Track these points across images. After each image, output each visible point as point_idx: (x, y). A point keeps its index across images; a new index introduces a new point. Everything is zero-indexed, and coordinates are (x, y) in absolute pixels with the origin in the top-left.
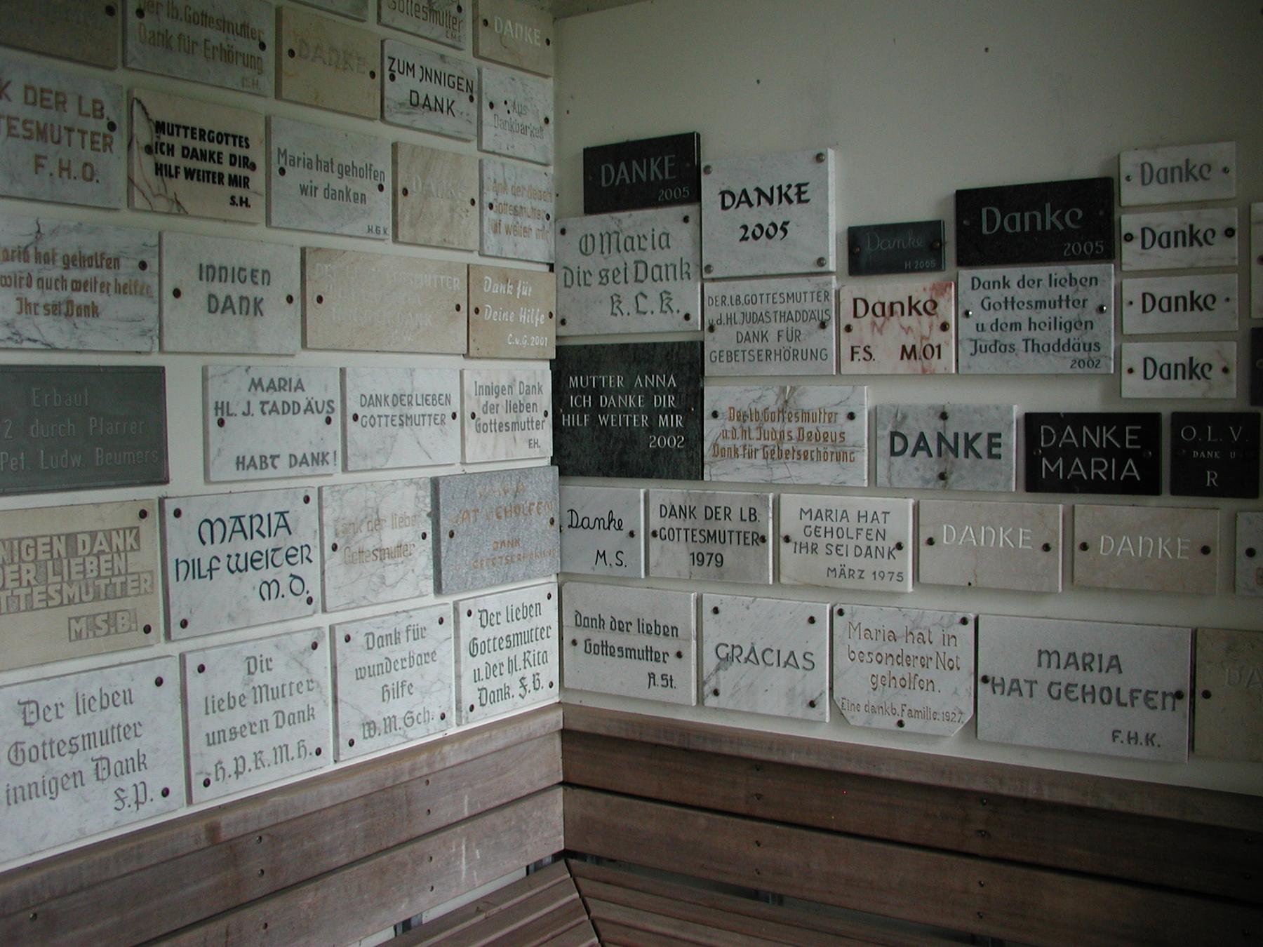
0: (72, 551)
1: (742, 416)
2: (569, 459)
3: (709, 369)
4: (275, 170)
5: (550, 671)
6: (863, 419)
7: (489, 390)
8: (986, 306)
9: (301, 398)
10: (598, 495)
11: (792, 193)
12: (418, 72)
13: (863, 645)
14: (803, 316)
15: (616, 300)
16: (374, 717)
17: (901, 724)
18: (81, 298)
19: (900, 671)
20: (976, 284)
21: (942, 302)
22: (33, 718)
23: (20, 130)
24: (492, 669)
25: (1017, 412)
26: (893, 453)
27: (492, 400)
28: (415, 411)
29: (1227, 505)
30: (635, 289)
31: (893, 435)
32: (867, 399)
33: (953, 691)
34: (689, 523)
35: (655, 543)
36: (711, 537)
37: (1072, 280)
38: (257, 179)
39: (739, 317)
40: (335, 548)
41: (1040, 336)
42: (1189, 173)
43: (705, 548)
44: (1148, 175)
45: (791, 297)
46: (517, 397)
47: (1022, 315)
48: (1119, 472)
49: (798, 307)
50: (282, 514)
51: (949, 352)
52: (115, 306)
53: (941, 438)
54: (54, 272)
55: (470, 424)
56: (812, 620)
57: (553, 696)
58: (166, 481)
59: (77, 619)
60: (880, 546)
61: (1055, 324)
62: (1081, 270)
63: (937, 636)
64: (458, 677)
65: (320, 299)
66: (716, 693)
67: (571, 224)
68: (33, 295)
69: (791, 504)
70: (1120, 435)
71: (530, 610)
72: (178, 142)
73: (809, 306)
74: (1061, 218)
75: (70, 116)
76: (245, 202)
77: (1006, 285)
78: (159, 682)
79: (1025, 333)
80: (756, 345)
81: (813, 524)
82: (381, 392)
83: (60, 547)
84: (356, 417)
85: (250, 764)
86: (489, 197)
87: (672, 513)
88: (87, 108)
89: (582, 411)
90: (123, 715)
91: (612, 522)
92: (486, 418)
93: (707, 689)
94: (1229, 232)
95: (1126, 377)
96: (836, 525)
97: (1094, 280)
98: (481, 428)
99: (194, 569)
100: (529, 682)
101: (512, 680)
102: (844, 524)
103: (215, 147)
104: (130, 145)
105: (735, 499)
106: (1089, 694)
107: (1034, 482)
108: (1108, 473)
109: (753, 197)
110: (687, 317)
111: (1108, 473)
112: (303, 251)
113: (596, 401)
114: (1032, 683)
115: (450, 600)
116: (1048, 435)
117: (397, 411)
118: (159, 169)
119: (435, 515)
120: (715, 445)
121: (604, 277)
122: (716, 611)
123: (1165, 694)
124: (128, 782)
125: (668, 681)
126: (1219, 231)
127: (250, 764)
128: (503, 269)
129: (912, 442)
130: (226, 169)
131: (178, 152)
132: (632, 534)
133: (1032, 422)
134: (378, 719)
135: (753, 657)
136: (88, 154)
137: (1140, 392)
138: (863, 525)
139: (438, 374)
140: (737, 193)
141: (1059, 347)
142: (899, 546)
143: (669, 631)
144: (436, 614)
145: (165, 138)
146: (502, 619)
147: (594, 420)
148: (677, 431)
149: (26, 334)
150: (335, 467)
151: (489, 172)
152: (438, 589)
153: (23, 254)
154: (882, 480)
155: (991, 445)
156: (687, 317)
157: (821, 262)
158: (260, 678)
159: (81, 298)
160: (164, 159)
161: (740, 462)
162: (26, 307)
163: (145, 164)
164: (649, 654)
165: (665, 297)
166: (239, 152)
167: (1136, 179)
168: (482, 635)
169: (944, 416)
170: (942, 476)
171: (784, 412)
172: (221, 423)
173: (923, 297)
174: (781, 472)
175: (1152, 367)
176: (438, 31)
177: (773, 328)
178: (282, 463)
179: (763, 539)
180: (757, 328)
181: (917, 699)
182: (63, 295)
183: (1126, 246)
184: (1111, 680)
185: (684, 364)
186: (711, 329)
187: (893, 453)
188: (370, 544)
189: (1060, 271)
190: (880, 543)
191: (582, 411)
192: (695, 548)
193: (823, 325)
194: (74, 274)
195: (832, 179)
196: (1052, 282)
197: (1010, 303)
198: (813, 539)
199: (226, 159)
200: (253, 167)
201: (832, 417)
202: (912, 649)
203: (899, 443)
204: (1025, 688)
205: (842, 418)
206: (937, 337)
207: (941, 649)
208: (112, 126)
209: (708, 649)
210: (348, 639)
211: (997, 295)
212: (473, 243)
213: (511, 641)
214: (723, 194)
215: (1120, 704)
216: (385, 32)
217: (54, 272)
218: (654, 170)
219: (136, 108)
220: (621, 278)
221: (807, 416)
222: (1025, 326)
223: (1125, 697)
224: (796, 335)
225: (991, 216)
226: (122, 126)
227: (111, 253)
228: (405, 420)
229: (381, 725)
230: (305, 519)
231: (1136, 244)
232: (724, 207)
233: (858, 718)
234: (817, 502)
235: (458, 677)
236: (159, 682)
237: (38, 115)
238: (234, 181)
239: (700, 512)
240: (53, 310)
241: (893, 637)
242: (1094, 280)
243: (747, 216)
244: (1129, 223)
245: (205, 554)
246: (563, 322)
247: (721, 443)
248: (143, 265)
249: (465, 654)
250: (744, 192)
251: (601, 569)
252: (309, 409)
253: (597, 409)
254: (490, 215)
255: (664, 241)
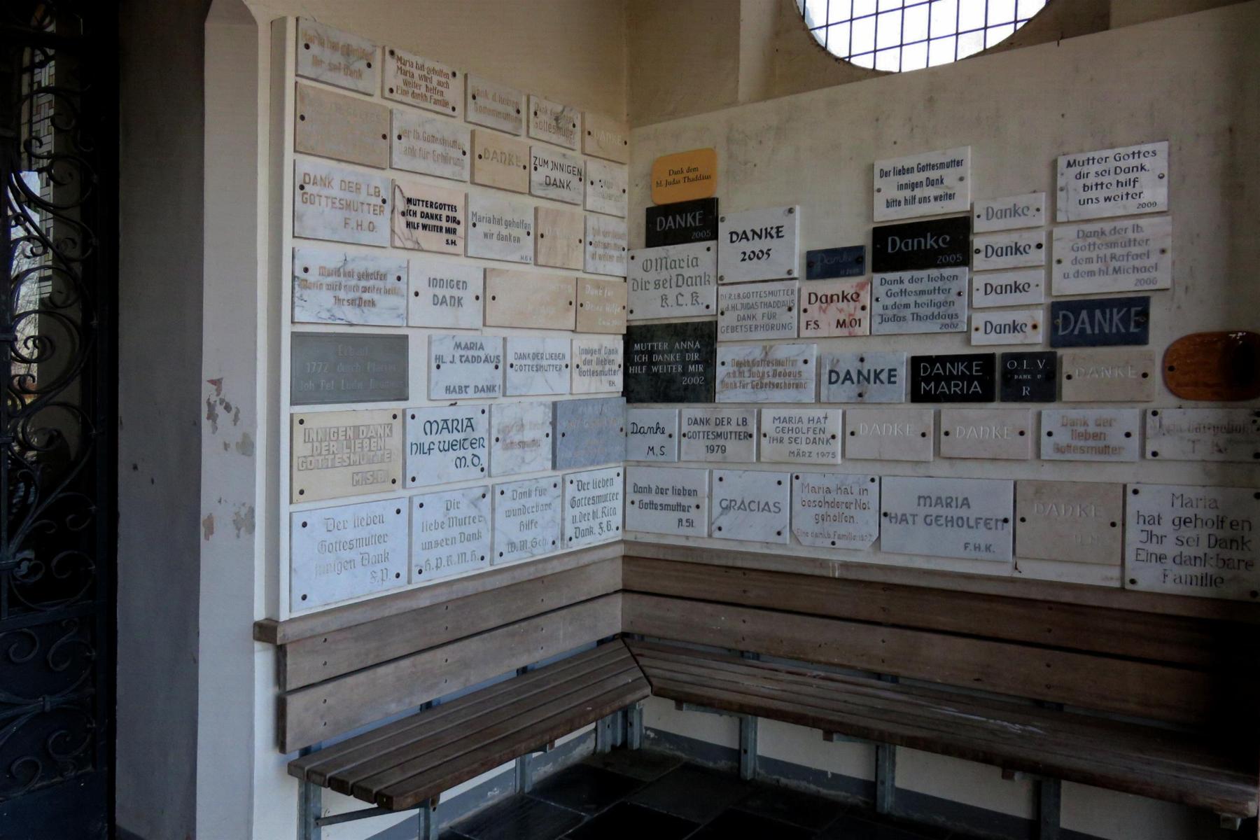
0: (357, 437)
1: (739, 364)
2: (631, 394)
3: (720, 337)
4: (470, 224)
5: (617, 520)
6: (813, 364)
7: (587, 351)
8: (889, 294)
9: (482, 354)
10: (650, 414)
11: (774, 232)
12: (550, 165)
13: (812, 497)
14: (777, 304)
15: (664, 298)
16: (514, 540)
17: (833, 543)
18: (366, 296)
19: (832, 512)
20: (883, 282)
21: (862, 294)
22: (331, 528)
23: (337, 204)
24: (584, 516)
25: (906, 356)
26: (830, 382)
27: (589, 357)
28: (545, 363)
29: (1033, 408)
30: (676, 291)
31: (831, 372)
32: (814, 351)
33: (867, 522)
34: (706, 428)
35: (684, 440)
36: (719, 435)
37: (942, 278)
38: (460, 229)
39: (739, 306)
40: (497, 440)
41: (923, 311)
42: (1016, 212)
43: (716, 442)
44: (990, 214)
45: (772, 293)
46: (603, 356)
47: (910, 300)
48: (969, 389)
49: (776, 299)
50: (469, 419)
51: (866, 323)
52: (384, 301)
53: (860, 373)
54: (353, 282)
55: (576, 371)
56: (779, 483)
57: (619, 535)
58: (406, 399)
59: (357, 473)
60: (820, 437)
61: (932, 304)
62: (947, 272)
63: (856, 490)
64: (563, 519)
65: (494, 298)
66: (720, 529)
67: (637, 253)
68: (342, 294)
69: (768, 414)
70: (969, 368)
71: (607, 482)
72: (419, 209)
73: (782, 298)
74: (936, 241)
75: (363, 197)
76: (454, 243)
77: (902, 282)
78: (398, 512)
79: (913, 309)
80: (749, 322)
81: (781, 426)
82: (526, 351)
83: (350, 433)
84: (512, 366)
85: (444, 562)
86: (589, 239)
87: (696, 422)
88: (372, 191)
89: (642, 364)
90: (377, 529)
91: (658, 429)
92: (584, 368)
93: (714, 527)
94: (1039, 246)
95: (973, 333)
96: (795, 426)
97: (955, 277)
98: (582, 374)
99: (420, 449)
100: (604, 526)
101: (594, 524)
102: (800, 425)
103: (438, 212)
104: (393, 211)
105: (734, 414)
106: (950, 521)
107: (917, 396)
108: (962, 390)
109: (750, 235)
110: (708, 307)
111: (962, 390)
112: (485, 270)
113: (650, 358)
114: (914, 516)
115: (559, 473)
116: (925, 369)
117: (535, 363)
118: (408, 224)
119: (554, 424)
120: (722, 381)
121: (657, 285)
122: (721, 479)
123: (997, 521)
124: (378, 567)
125: (690, 523)
126: (1033, 245)
127: (444, 562)
128: (596, 281)
129: (842, 376)
130: (444, 224)
131: (418, 214)
132: (670, 436)
133: (916, 362)
134: (517, 541)
135: (743, 506)
136: (372, 217)
137: (983, 342)
138: (811, 425)
139: (558, 343)
140: (740, 232)
141: (933, 317)
142: (833, 437)
143: (692, 493)
144: (553, 481)
145: (412, 207)
146: (590, 486)
147: (649, 369)
148: (700, 374)
149: (338, 315)
150: (498, 393)
151: (589, 224)
152: (554, 467)
153: (337, 272)
154: (823, 398)
155: (890, 376)
156: (708, 307)
157: (789, 272)
158: (453, 513)
159: (366, 296)
160: (411, 219)
161: (739, 391)
162: (338, 300)
163: (401, 222)
164: (680, 507)
165: (694, 296)
166: (451, 214)
167: (983, 217)
168: (579, 495)
169: (862, 360)
170: (860, 395)
171: (765, 361)
172: (438, 367)
173: (850, 291)
174: (762, 396)
175: (989, 327)
176: (561, 140)
177: (759, 312)
178: (471, 390)
179: (751, 436)
180: (749, 312)
181: (843, 528)
182: (357, 295)
183: (976, 257)
184: (963, 512)
185: (704, 336)
186: (722, 314)
187: (830, 382)
188: (517, 438)
189: (934, 272)
190: (822, 436)
191: (642, 364)
192: (709, 443)
193: (790, 309)
194: (363, 283)
195: (798, 223)
196: (930, 279)
197: (904, 292)
198: (781, 434)
199: (444, 218)
200: (459, 223)
201: (794, 363)
202: (841, 498)
203: (835, 377)
204: (910, 519)
205: (800, 363)
206: (859, 314)
207: (858, 498)
208: (384, 201)
209: (716, 502)
210: (502, 493)
211: (896, 288)
212: (580, 266)
213: (595, 500)
214: (731, 233)
215: (969, 527)
216: (531, 142)
217: (353, 282)
218: (690, 220)
219: (397, 191)
220: (667, 285)
221: (779, 363)
222: (912, 305)
223: (972, 523)
224: (774, 316)
225: (894, 242)
226: (389, 202)
227: (382, 271)
228: (539, 368)
229: (518, 545)
230: (481, 422)
231: (982, 254)
232: (732, 242)
233: (807, 541)
234: (784, 413)
235: (563, 519)
236: (398, 512)
237: (348, 196)
238: (448, 231)
239: (712, 422)
240: (352, 302)
241: (829, 491)
242: (955, 277)
243: (747, 246)
244: (978, 242)
245: (427, 440)
246: (631, 312)
247: (727, 380)
248: (399, 279)
249: (567, 505)
250: (744, 232)
251: (651, 457)
252: (486, 360)
253: (651, 363)
254: (590, 249)
255: (695, 262)
